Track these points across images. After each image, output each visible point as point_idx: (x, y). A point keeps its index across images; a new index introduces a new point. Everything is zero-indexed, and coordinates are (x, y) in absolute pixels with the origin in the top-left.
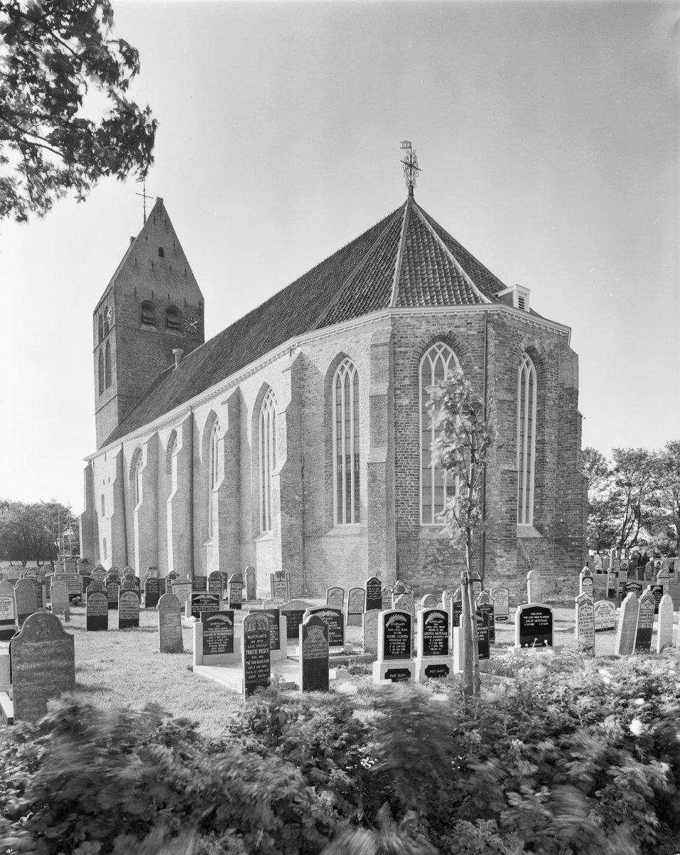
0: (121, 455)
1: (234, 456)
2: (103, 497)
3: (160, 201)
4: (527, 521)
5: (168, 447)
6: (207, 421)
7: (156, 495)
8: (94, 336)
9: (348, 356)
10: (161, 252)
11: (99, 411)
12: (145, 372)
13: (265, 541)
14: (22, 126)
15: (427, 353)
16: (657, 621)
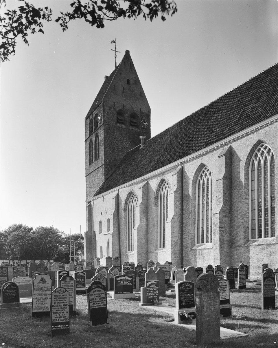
0: (117, 197)
1: (228, 191)
2: (100, 222)
3: (128, 52)
5: (157, 190)
6: (196, 171)
7: (147, 219)
8: (86, 132)
10: (128, 82)
11: (88, 175)
12: (119, 151)
13: (259, 245)
14: (25, 32)
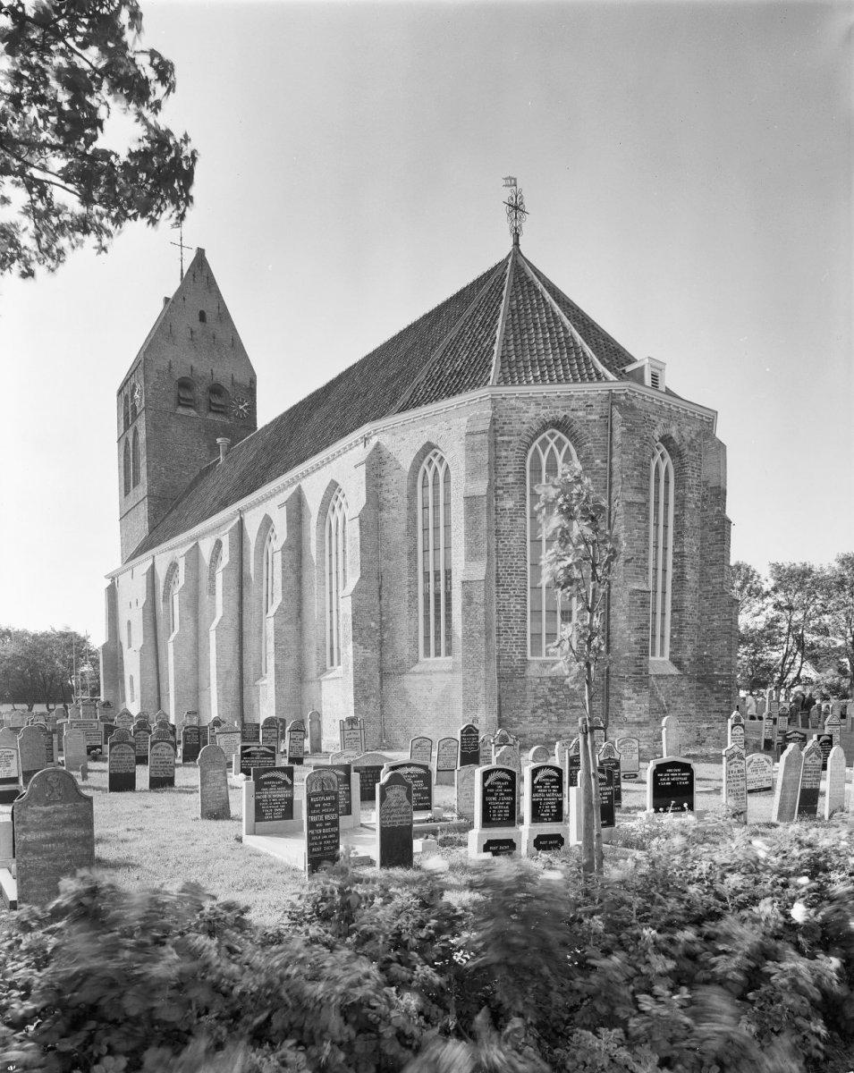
0: (152, 571)
1: (294, 573)
2: (129, 623)
3: (201, 252)
4: (662, 654)
6: (260, 529)
7: (196, 621)
8: (118, 422)
9: (437, 447)
10: (202, 316)
11: (124, 516)
12: (182, 466)
13: (333, 679)
14: (27, 158)
15: (536, 443)
16: (825, 779)
